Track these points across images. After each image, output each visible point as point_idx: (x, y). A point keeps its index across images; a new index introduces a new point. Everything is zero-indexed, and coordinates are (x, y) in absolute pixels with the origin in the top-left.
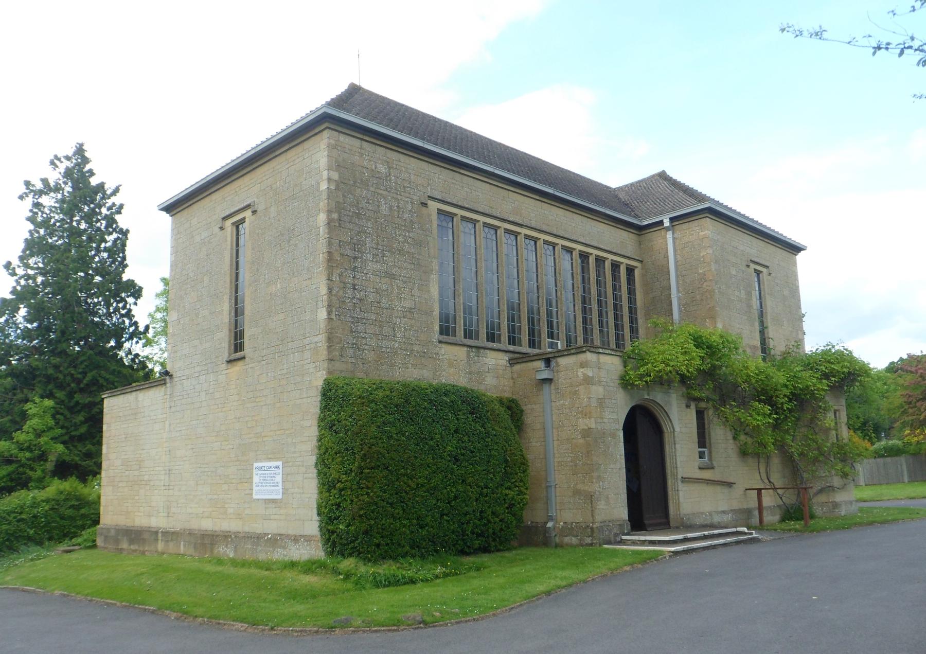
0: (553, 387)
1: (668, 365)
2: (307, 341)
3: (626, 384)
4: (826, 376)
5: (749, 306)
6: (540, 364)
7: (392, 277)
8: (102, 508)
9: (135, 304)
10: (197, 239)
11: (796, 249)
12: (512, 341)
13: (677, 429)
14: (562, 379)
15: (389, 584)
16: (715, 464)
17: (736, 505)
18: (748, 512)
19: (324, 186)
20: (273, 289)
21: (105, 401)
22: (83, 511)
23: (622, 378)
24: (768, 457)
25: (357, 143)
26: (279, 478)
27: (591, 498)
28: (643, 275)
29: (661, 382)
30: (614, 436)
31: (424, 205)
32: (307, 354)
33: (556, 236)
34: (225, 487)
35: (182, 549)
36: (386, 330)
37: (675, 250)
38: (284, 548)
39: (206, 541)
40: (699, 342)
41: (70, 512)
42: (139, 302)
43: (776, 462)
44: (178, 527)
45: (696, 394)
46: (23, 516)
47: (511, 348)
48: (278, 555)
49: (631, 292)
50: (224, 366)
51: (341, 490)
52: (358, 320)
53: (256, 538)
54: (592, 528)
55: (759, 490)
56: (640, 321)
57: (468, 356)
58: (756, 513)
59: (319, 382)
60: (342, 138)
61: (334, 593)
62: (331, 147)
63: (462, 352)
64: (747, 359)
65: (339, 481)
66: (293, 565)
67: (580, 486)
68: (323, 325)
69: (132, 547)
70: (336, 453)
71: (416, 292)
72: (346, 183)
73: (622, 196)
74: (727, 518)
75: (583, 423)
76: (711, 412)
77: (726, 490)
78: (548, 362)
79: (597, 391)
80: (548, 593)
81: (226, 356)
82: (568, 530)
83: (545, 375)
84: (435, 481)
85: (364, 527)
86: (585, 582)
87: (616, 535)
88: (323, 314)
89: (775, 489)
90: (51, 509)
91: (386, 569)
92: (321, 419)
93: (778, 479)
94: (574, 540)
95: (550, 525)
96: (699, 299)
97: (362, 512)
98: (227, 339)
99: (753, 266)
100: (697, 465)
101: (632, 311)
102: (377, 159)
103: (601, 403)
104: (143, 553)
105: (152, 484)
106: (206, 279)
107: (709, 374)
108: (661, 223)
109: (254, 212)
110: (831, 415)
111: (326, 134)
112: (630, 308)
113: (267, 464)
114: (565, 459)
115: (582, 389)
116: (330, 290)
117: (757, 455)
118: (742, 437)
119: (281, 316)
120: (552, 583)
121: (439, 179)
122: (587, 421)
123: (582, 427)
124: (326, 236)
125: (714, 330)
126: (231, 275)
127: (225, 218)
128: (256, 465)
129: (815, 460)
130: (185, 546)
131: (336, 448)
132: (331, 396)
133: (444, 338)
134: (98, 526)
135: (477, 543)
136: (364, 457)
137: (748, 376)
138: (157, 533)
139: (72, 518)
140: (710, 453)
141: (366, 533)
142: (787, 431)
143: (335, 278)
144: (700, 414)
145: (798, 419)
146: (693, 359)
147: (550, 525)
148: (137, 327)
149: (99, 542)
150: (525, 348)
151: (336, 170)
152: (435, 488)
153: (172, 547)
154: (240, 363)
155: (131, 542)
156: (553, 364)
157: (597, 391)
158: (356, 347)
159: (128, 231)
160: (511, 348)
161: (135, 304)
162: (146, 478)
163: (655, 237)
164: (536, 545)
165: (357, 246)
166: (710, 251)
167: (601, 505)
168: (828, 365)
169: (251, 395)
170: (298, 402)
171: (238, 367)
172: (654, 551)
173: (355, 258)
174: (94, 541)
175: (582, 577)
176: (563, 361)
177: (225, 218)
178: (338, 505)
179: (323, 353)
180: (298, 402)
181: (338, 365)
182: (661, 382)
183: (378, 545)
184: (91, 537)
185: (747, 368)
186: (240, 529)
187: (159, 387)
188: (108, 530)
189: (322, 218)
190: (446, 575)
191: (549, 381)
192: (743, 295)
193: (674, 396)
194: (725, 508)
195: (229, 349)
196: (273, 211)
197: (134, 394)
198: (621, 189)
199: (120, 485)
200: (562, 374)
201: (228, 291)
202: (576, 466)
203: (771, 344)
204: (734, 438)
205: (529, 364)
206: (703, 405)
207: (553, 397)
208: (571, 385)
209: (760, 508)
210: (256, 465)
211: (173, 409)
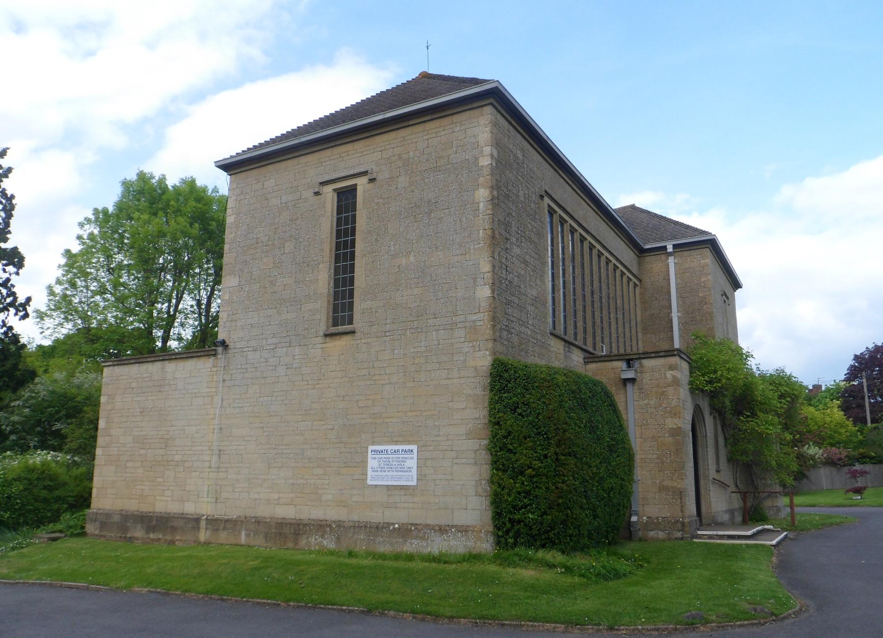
2: (458, 319)
6: (622, 365)
8: (94, 491)
9: (17, 274)
10: (274, 202)
14: (646, 379)
21: (105, 370)
22: (57, 493)
32: (460, 333)
35: (243, 539)
39: (289, 531)
41: (44, 493)
42: (21, 271)
44: (234, 514)
48: (411, 546)
50: (320, 339)
51: (531, 477)
53: (377, 529)
54: (683, 524)
59: (484, 361)
65: (529, 468)
67: (665, 483)
68: (484, 304)
69: (151, 536)
70: (525, 438)
81: (322, 329)
82: (654, 524)
83: (630, 375)
88: (484, 292)
90: (26, 489)
97: (560, 501)
104: (172, 542)
105: (187, 464)
106: (289, 246)
108: (665, 248)
109: (372, 180)
113: (390, 448)
114: (650, 456)
115: (670, 390)
119: (416, 291)
122: (676, 421)
123: (670, 426)
124: (489, 212)
126: (331, 244)
127: (323, 184)
128: (371, 448)
130: (248, 535)
134: (87, 511)
138: (197, 520)
139: (45, 500)
141: (564, 522)
143: (496, 257)
148: (15, 299)
149: (90, 528)
155: (150, 529)
159: (13, 197)
161: (17, 274)
162: (178, 458)
163: (654, 264)
165: (507, 225)
169: (364, 372)
170: (444, 382)
171: (342, 342)
172: (733, 544)
174: (83, 528)
177: (323, 184)
178: (528, 493)
179: (487, 331)
180: (444, 382)
183: (570, 536)
184: (80, 523)
186: (344, 517)
187: (204, 359)
188: (108, 515)
189: (483, 194)
191: (633, 380)
195: (328, 322)
196: (403, 181)
197: (159, 364)
199: (130, 464)
201: (327, 259)
202: (663, 463)
208: (658, 386)
210: (371, 448)
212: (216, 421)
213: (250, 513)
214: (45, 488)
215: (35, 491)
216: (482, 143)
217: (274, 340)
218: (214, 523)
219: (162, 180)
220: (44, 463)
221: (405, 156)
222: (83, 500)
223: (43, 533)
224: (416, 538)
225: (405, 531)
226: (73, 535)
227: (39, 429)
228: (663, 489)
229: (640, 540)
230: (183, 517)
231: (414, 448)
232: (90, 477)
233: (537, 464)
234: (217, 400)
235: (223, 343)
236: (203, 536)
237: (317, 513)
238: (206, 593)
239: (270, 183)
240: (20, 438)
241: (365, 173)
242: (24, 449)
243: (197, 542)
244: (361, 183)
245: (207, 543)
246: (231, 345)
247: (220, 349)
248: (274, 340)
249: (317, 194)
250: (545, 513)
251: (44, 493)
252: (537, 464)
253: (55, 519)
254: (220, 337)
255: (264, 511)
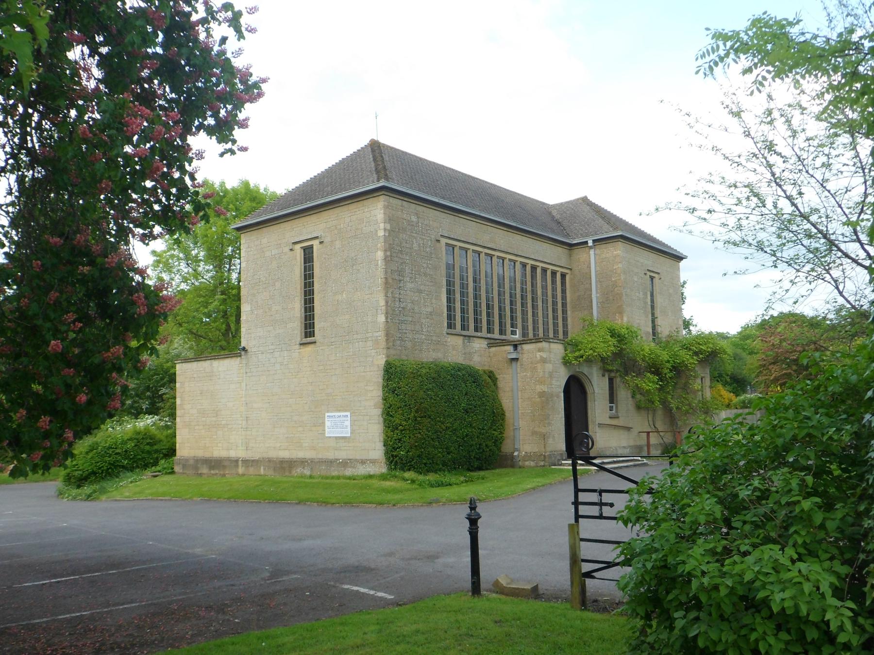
0: (519, 364)
1: (594, 351)
2: (370, 335)
3: (566, 363)
4: (696, 354)
5: (646, 303)
6: (510, 348)
7: (420, 291)
8: (177, 445)
10: (268, 254)
11: (679, 258)
12: (489, 331)
13: (596, 391)
15: (439, 486)
16: (620, 415)
17: (632, 443)
18: (640, 448)
19: (381, 233)
20: (339, 297)
21: (177, 366)
22: (156, 447)
23: (564, 358)
24: (654, 410)
25: (399, 202)
26: (348, 423)
27: (544, 437)
28: (571, 280)
29: (589, 361)
30: (558, 397)
31: (438, 241)
32: (370, 343)
33: (517, 255)
34: (300, 429)
35: (262, 472)
36: (418, 327)
37: (596, 263)
38: (353, 467)
39: (285, 465)
40: (613, 333)
41: (147, 448)
43: (660, 413)
45: (610, 368)
46: (118, 451)
47: (489, 336)
48: (349, 472)
49: (564, 291)
50: (297, 347)
51: (402, 431)
52: (402, 322)
53: (330, 462)
55: (648, 433)
56: (569, 313)
57: (464, 343)
58: (646, 448)
59: (381, 361)
60: (391, 200)
61: (408, 490)
62: (386, 207)
63: (459, 341)
64: (644, 346)
66: (371, 477)
68: (382, 326)
69: (212, 472)
71: (434, 301)
72: (395, 229)
73: (554, 213)
74: (626, 452)
75: (540, 388)
76: (618, 379)
77: (626, 433)
78: (515, 347)
79: (549, 367)
80: (534, 489)
82: (528, 457)
83: (514, 356)
84: (456, 425)
85: (418, 453)
86: (551, 484)
87: (559, 460)
88: (382, 319)
89: (658, 432)
90: (136, 446)
91: (432, 477)
92: (384, 387)
93: (660, 426)
94: (532, 464)
95: (516, 454)
96: (613, 298)
98: (299, 328)
99: (649, 273)
100: (608, 415)
101: (564, 305)
102: (410, 212)
103: (551, 375)
104: (224, 475)
106: (278, 284)
107: (619, 355)
108: (586, 243)
109: (321, 243)
110: (699, 381)
111: (382, 198)
112: (553, 288)
113: (337, 414)
115: (539, 365)
116: (387, 302)
117: (647, 409)
118: (638, 396)
119: (347, 317)
120: (534, 485)
121: (444, 223)
125: (622, 322)
128: (327, 414)
129: (687, 412)
130: (264, 469)
131: (398, 405)
132: (391, 372)
133: (450, 331)
135: (476, 464)
136: (417, 412)
137: (644, 356)
138: (237, 461)
139: (149, 452)
140: (617, 407)
141: (419, 456)
142: (668, 393)
143: (390, 295)
144: (611, 381)
145: (676, 384)
146: (609, 346)
147: (516, 454)
149: (177, 469)
150: (496, 335)
151: (389, 223)
152: (455, 430)
153: (252, 470)
154: (312, 346)
155: (211, 468)
156: (519, 348)
157: (549, 367)
158: (401, 339)
160: (489, 336)
162: (223, 422)
163: (580, 255)
164: (506, 467)
165: (400, 272)
166: (620, 265)
167: (550, 441)
168: (697, 346)
169: (322, 367)
170: (363, 374)
171: (310, 348)
173: (400, 281)
175: (548, 481)
176: (526, 347)
178: (400, 440)
179: (383, 344)
180: (363, 374)
181: (392, 352)
182: (589, 361)
183: (425, 464)
185: (643, 350)
186: (314, 457)
188: (187, 460)
189: (380, 255)
190: (466, 482)
191: (516, 359)
192: (641, 295)
193: (595, 369)
194: (625, 445)
196: (338, 244)
197: (208, 362)
198: (553, 206)
199: (197, 427)
200: (525, 355)
201: (299, 294)
203: (659, 329)
204: (633, 397)
205: (502, 348)
206: (613, 375)
207: (519, 371)
208: (532, 363)
209: (648, 445)
210: (327, 414)
211: (249, 374)
212: (243, 399)
213: (265, 456)
214: (148, 444)
215: (142, 446)
216: (379, 221)
217: (272, 347)
218: (246, 462)
219: (222, 184)
220: (146, 428)
221: (338, 227)
222: (171, 452)
223: (148, 473)
224: (351, 467)
225: (345, 463)
226: (167, 473)
227: (148, 393)
228: (534, 433)
229: (520, 467)
230: (229, 459)
231: (348, 414)
232: (174, 436)
233: (404, 423)
234: (243, 385)
235: (244, 349)
236: (241, 470)
237: (301, 455)
238: (229, 498)
239: (265, 241)
240: (135, 402)
241: (317, 238)
242: (137, 414)
243: (238, 474)
244: (315, 243)
245: (243, 475)
246: (249, 350)
247: (243, 353)
248: (272, 347)
249: (291, 250)
250: (408, 451)
251: (147, 448)
252: (404, 423)
253: (155, 464)
254: (243, 345)
255: (273, 454)
